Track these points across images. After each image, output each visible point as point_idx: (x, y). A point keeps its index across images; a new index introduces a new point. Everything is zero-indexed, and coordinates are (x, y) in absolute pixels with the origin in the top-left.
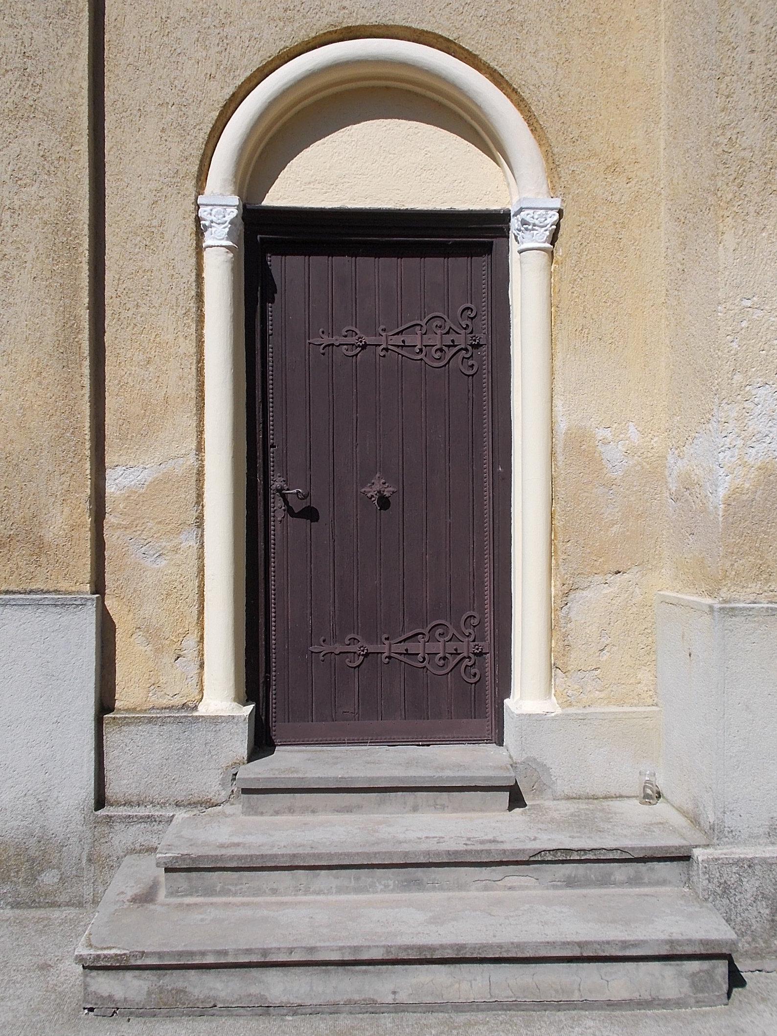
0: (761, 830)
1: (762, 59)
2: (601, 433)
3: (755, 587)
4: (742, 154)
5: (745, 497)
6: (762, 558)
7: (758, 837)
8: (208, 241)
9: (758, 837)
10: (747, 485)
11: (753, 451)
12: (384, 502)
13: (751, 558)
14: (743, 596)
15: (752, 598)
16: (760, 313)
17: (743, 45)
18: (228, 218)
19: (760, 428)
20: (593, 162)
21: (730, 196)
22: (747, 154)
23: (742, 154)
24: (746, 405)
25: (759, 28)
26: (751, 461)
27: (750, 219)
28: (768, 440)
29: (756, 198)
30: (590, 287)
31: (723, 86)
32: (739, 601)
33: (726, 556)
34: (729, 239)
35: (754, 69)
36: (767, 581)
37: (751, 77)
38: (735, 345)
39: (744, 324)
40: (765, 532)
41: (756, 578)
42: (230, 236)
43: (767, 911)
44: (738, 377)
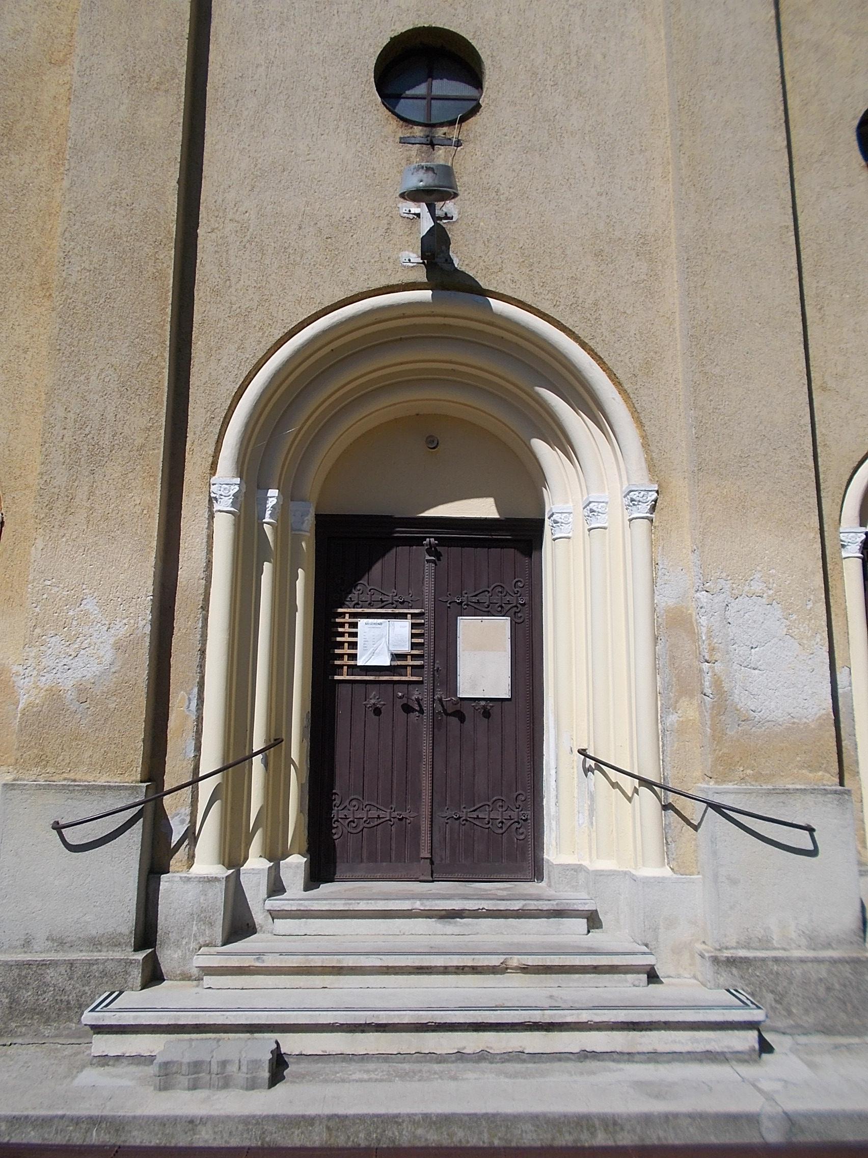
0: (18, 943)
1: (71, 433)
2: (15, 668)
3: (36, 770)
4: (53, 490)
5: (35, 709)
6: (42, 750)
7: (16, 947)
8: (216, 507)
9: (16, 947)
10: (37, 701)
11: (44, 679)
12: (377, 711)
13: (36, 751)
14: (29, 777)
15: (34, 778)
16: (57, 589)
17: (59, 425)
18: (232, 492)
19: (50, 663)
20: (27, 492)
21: (43, 516)
22: (57, 490)
23: (53, 490)
24: (42, 648)
25: (71, 415)
26: (41, 685)
27: (55, 530)
28: (55, 671)
29: (60, 517)
30: (18, 572)
31: (44, 449)
32: (24, 780)
33: (18, 749)
34: (40, 544)
35: (65, 439)
36: (45, 766)
37: (62, 444)
38: (37, 609)
39: (45, 596)
40: (47, 733)
41: (37, 765)
42: (233, 504)
43: (7, 1001)
44: (38, 630)
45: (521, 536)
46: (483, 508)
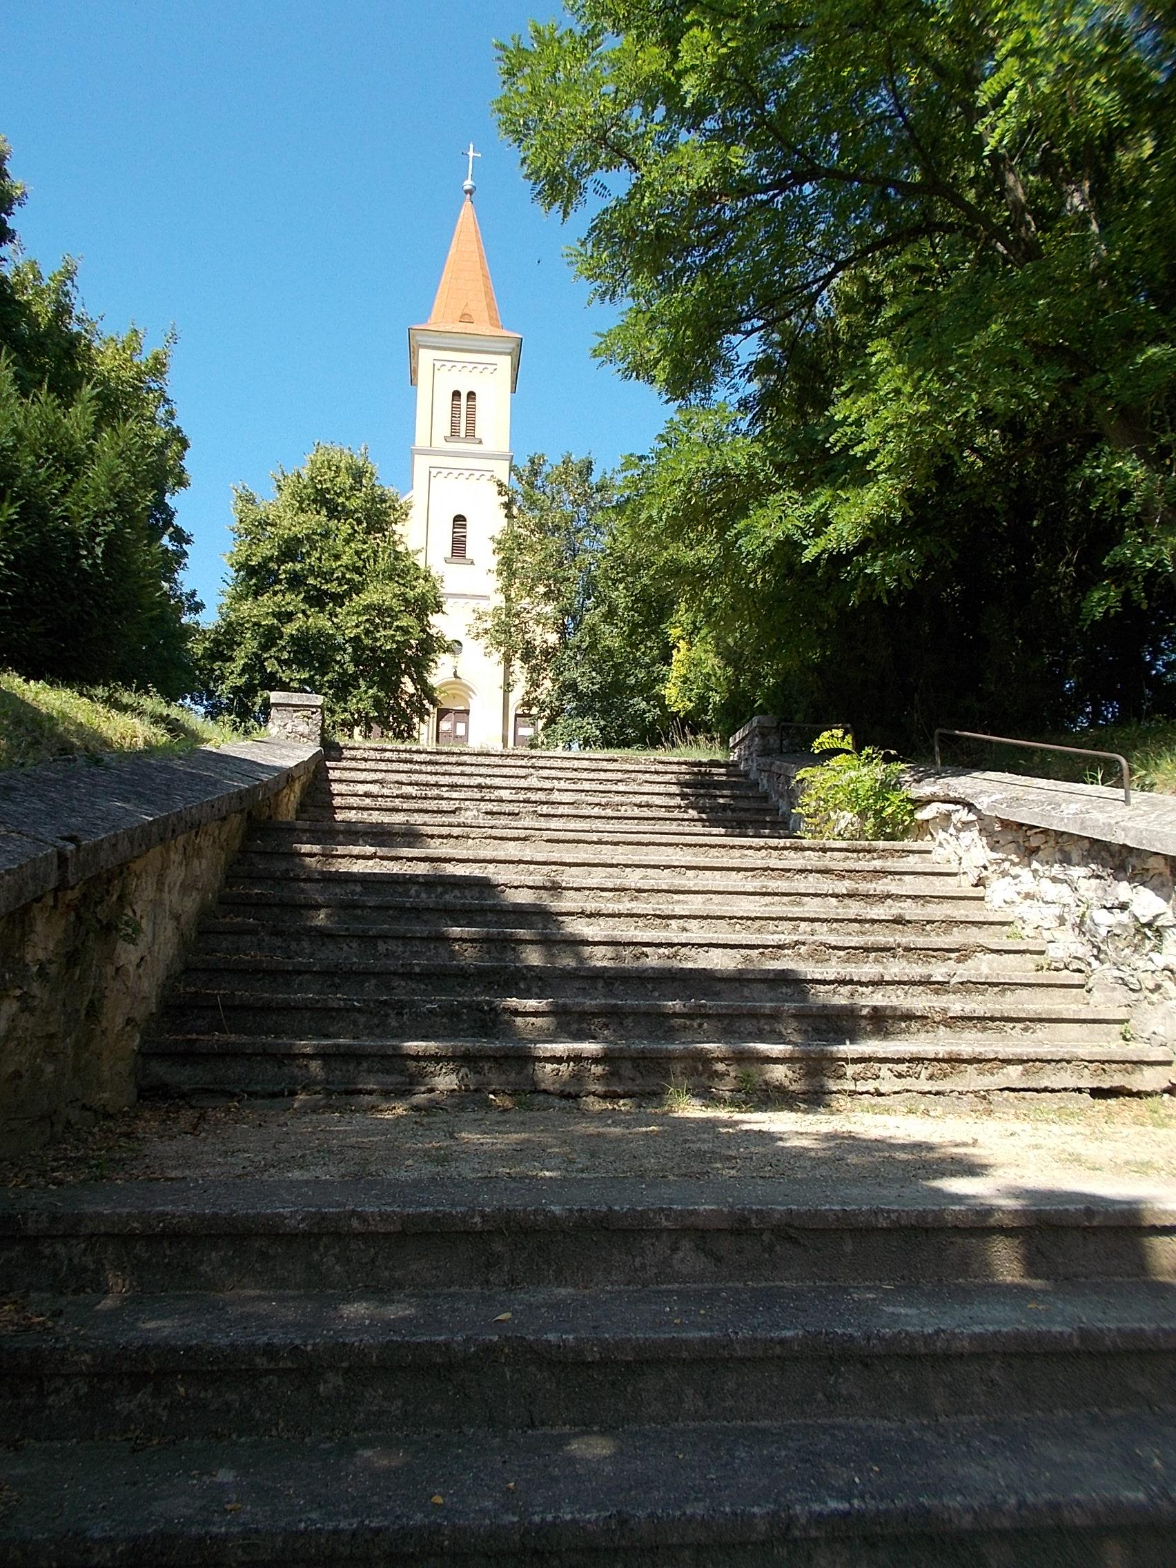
45: (467, 712)
46: (462, 708)
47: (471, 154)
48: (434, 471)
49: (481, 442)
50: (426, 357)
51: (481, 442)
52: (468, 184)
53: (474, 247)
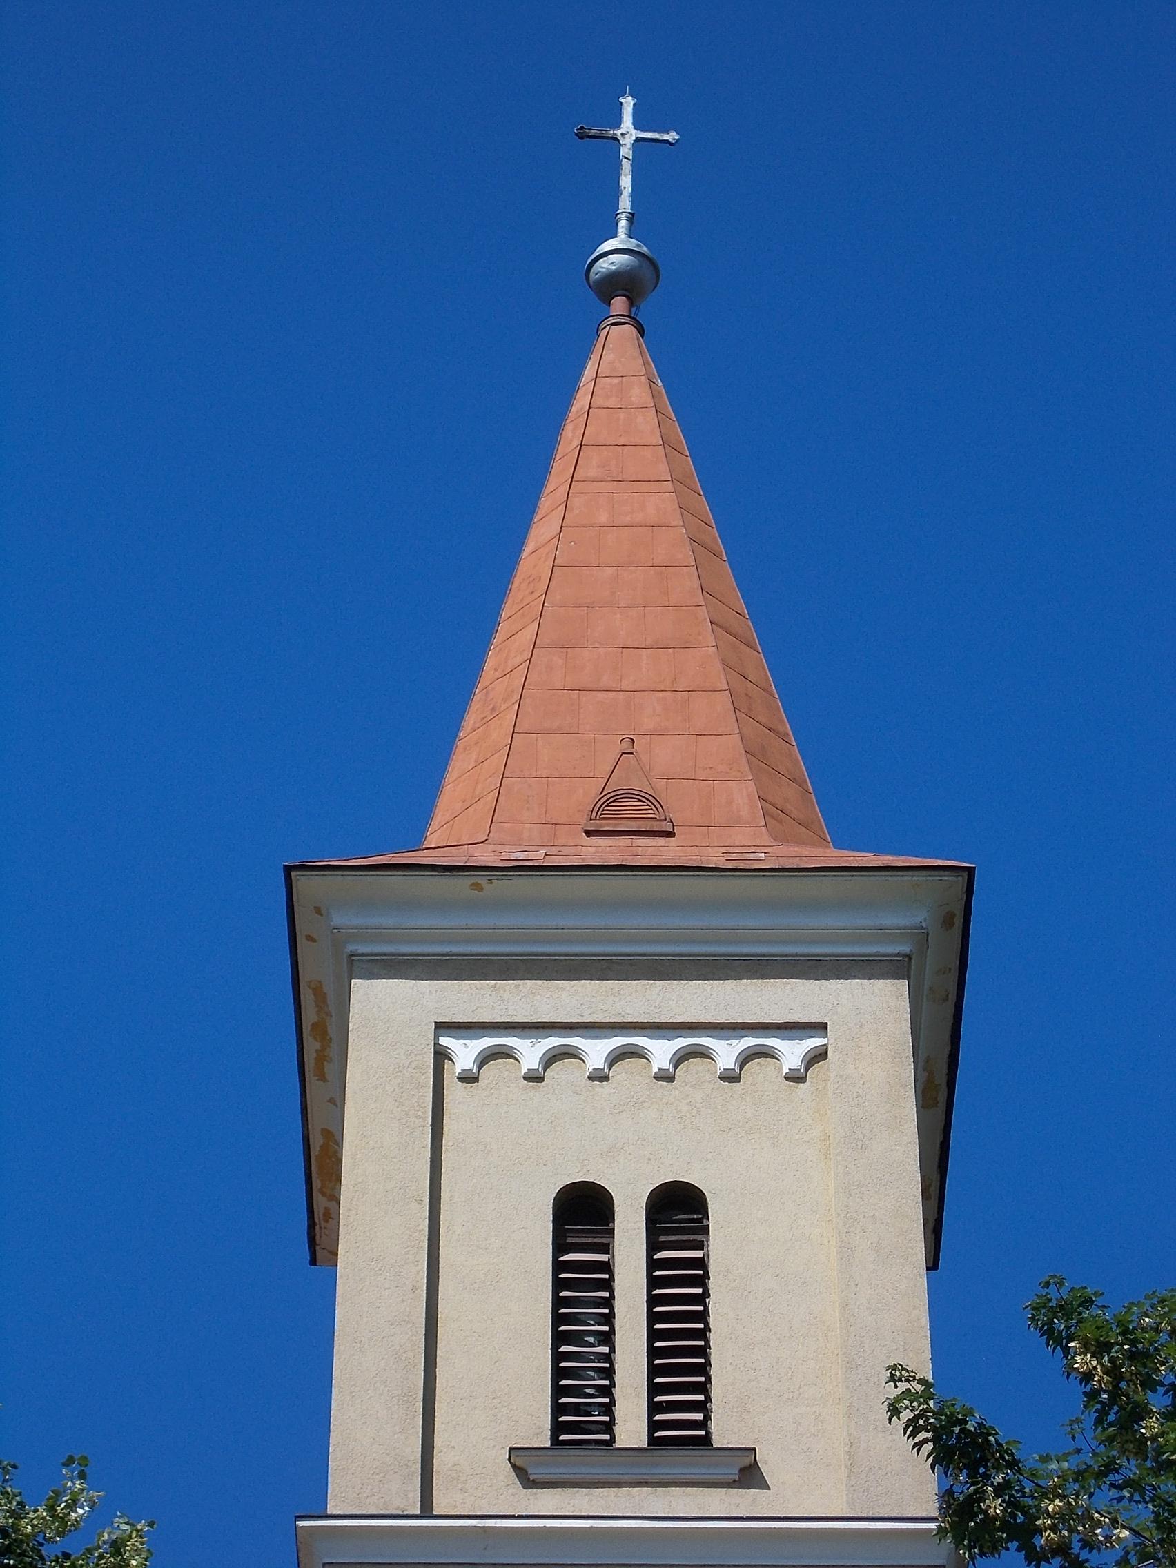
47: (628, 132)
48: (465, 1053)
49: (749, 1474)
50: (388, 1019)
51: (749, 1474)
52: (615, 252)
53: (661, 504)
